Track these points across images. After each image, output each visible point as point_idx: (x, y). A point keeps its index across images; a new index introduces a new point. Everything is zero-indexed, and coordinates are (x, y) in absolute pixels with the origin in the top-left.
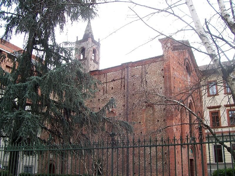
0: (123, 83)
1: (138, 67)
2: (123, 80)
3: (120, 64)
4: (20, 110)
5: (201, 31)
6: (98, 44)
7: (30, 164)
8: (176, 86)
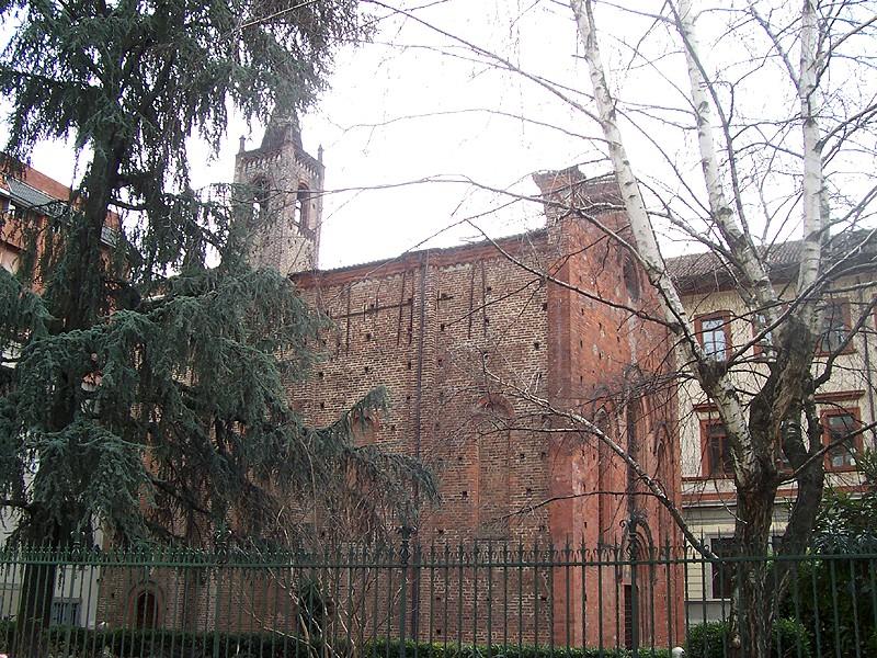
0: (406, 320)
1: (460, 267)
2: (407, 310)
3: (396, 254)
4: (81, 425)
5: (650, 258)
6: (315, 166)
7: (76, 595)
8: (586, 338)
